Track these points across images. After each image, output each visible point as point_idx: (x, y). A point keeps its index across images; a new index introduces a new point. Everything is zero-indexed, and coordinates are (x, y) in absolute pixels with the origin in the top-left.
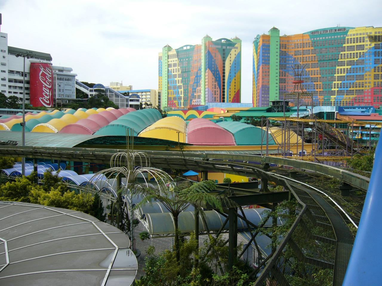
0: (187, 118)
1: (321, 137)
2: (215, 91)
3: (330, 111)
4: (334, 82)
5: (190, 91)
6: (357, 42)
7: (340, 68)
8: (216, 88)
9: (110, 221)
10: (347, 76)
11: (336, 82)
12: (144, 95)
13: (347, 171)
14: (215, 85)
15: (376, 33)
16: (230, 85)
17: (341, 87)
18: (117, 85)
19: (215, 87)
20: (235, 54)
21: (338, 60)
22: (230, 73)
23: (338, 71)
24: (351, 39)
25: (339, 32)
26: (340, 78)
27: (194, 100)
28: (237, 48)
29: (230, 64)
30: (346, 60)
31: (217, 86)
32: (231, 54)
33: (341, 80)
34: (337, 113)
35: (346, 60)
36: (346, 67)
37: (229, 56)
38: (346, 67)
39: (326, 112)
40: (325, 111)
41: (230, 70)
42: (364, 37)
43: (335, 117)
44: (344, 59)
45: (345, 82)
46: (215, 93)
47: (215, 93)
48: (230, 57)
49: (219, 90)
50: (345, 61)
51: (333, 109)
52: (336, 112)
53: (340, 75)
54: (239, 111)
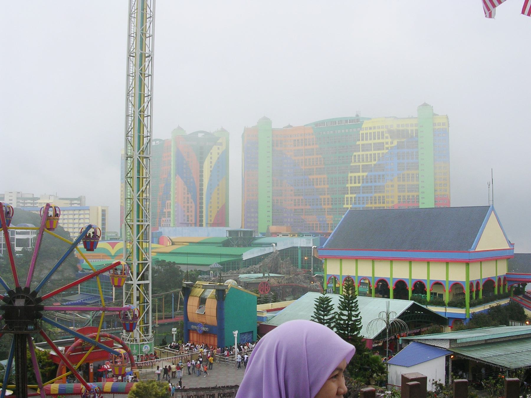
0: (116, 253)
1: (262, 289)
2: (188, 207)
3: (305, 246)
4: (346, 196)
5: (159, 204)
6: (375, 139)
7: (353, 175)
8: (190, 203)
9: (131, 388)
10: (363, 187)
11: (349, 196)
12: (82, 214)
13: (41, 378)
14: (188, 198)
15: (398, 126)
16: (211, 198)
17: (355, 203)
18: (49, 199)
19: (188, 200)
20: (218, 154)
21: (351, 164)
22: (210, 180)
23: (351, 180)
24: (367, 134)
25: (351, 123)
26: (354, 190)
27: (164, 219)
28: (221, 144)
29: (211, 167)
30: (361, 164)
31: (191, 200)
32: (211, 154)
33: (355, 193)
34: (314, 248)
35: (361, 164)
36: (361, 174)
37: (209, 155)
38: (361, 174)
39: (300, 247)
40: (299, 246)
41: (211, 176)
42: (383, 132)
43: (312, 255)
44: (367, 162)
45: (361, 195)
46: (188, 209)
47: (188, 209)
48: (211, 158)
49: (193, 205)
50: (359, 166)
51: (310, 242)
52: (313, 247)
53: (353, 185)
54: (188, 244)
